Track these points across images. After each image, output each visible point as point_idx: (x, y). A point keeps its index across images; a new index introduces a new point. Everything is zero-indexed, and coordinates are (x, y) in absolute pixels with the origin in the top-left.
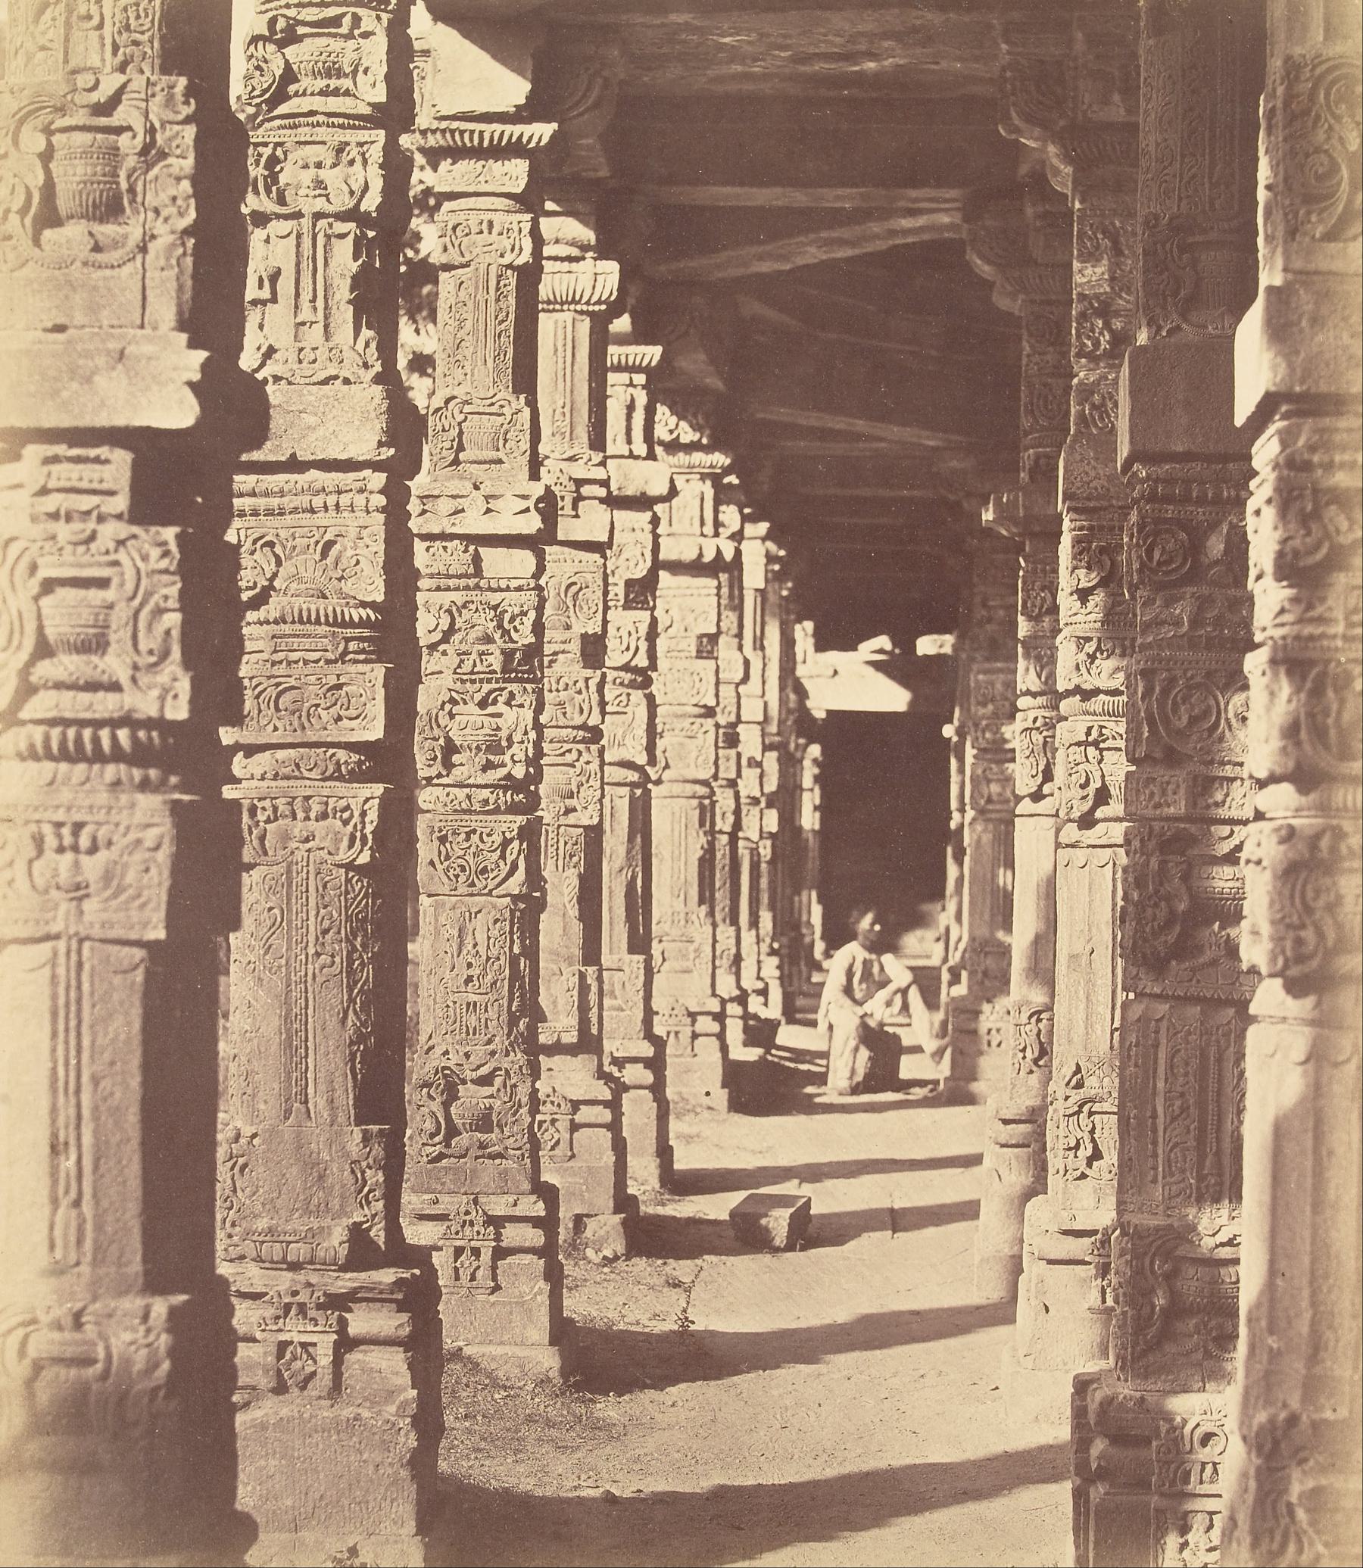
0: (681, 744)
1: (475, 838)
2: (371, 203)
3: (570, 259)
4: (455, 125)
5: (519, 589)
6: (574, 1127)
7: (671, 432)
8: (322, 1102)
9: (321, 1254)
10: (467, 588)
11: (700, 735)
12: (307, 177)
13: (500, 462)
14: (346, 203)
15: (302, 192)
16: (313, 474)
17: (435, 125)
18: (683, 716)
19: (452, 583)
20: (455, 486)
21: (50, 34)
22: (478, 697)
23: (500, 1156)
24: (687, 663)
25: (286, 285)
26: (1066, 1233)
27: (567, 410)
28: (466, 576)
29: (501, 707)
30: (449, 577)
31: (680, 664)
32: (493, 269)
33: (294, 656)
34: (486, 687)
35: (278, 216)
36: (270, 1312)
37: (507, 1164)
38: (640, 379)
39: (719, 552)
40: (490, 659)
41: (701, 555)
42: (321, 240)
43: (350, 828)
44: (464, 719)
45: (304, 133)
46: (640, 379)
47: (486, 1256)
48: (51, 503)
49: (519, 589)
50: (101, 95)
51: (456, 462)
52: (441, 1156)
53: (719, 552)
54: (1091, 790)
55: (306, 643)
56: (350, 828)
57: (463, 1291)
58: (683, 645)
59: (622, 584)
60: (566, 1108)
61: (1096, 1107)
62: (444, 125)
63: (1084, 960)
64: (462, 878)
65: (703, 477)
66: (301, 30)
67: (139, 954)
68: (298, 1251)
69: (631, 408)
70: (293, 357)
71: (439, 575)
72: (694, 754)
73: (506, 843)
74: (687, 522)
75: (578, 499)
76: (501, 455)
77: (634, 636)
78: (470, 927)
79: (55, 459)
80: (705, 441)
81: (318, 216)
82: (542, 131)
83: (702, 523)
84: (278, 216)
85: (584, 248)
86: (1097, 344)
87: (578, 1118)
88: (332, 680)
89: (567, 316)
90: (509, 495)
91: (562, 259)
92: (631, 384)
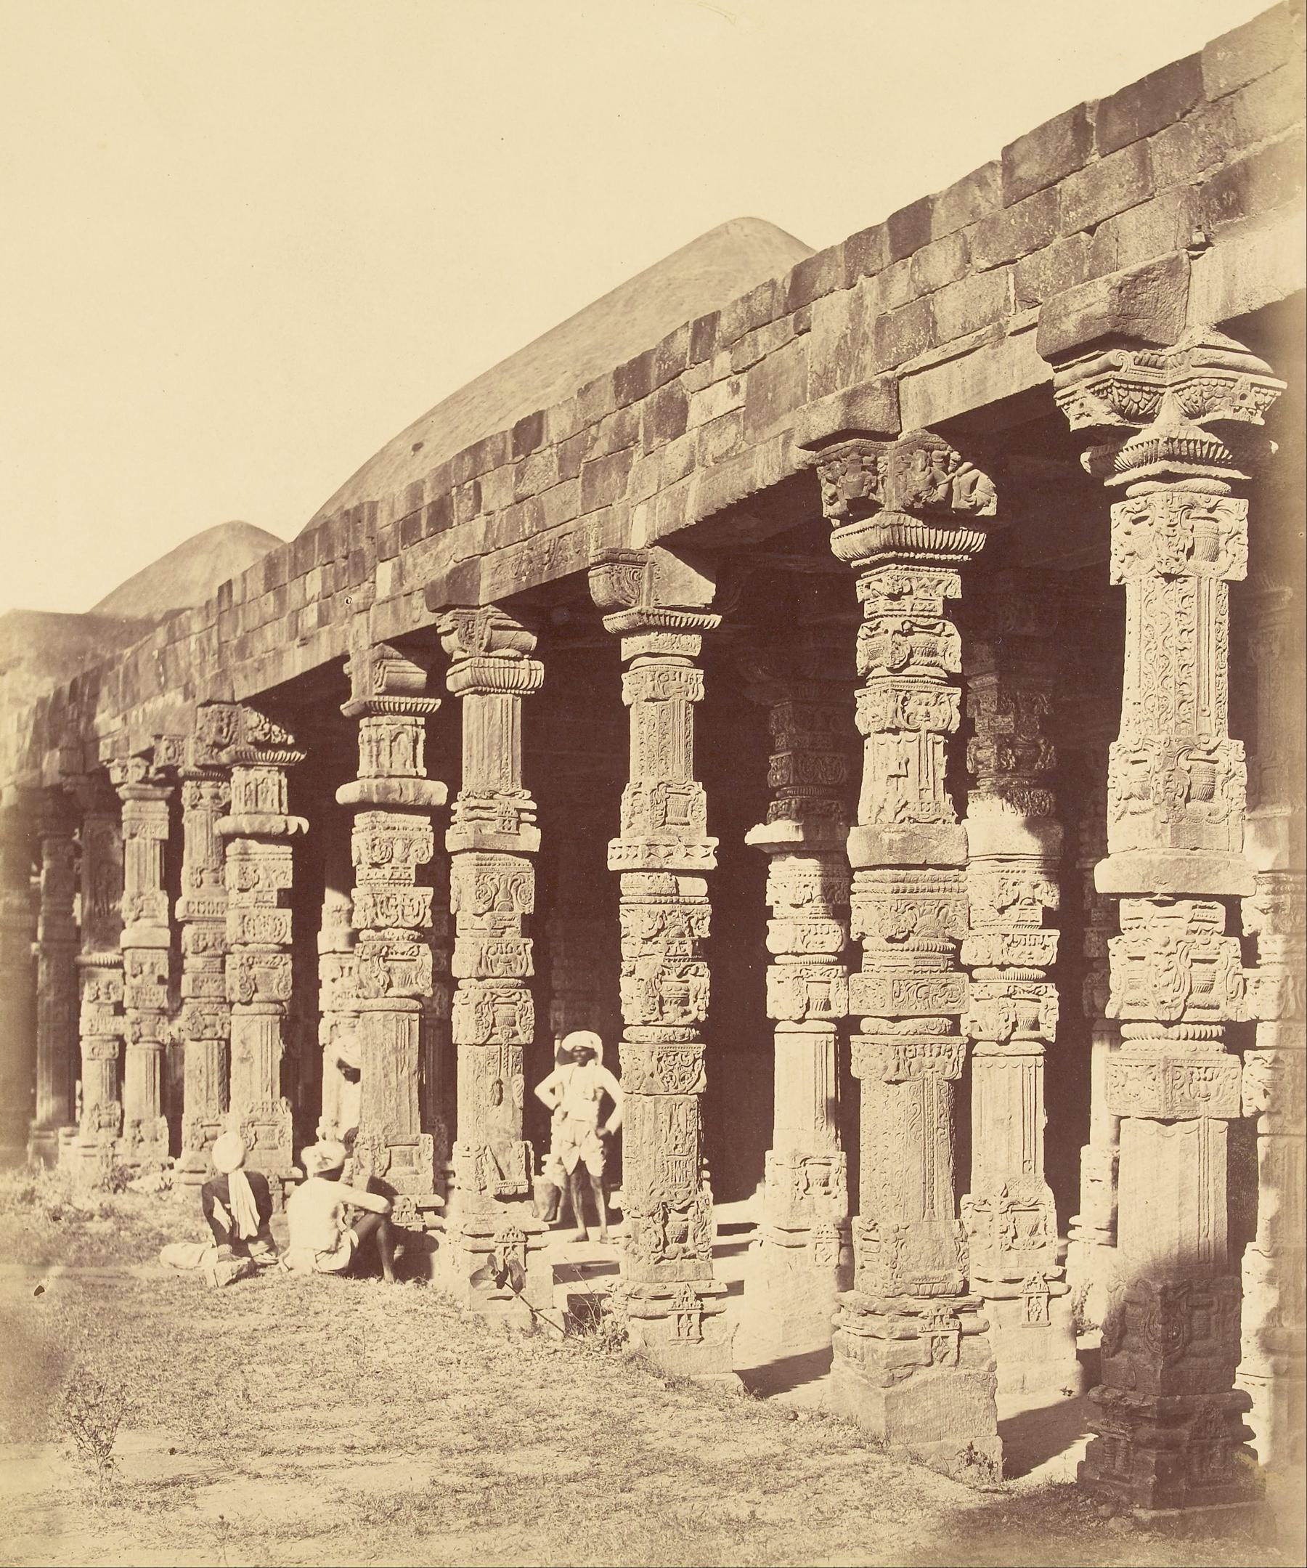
0: (267, 973)
1: (678, 1058)
2: (954, 727)
3: (515, 659)
4: (669, 612)
5: (700, 903)
6: (527, 1250)
7: (265, 735)
8: (941, 1207)
9: (950, 1287)
10: (672, 902)
11: (281, 967)
12: (922, 710)
13: (688, 824)
14: (941, 726)
15: (918, 717)
16: (930, 871)
17: (656, 611)
18: (268, 952)
19: (663, 899)
20: (666, 839)
21: (1189, 716)
22: (679, 970)
23: (694, 1256)
24: (271, 912)
25: (913, 767)
26: (1006, 1281)
27: (509, 761)
28: (671, 895)
29: (689, 977)
30: (660, 895)
31: (265, 912)
32: (683, 702)
33: (925, 968)
34: (683, 965)
35: (906, 729)
36: (927, 1321)
37: (697, 1261)
38: (421, 721)
39: (300, 826)
40: (684, 947)
41: (287, 829)
42: (930, 743)
43: (952, 1060)
44: (670, 984)
45: (919, 686)
46: (421, 721)
47: (696, 1318)
48: (1195, 926)
49: (700, 903)
50: (1210, 747)
51: (664, 824)
52: (662, 1258)
53: (300, 826)
54: (1010, 1023)
55: (931, 962)
56: (952, 1060)
57: (683, 1343)
58: (267, 897)
59: (413, 868)
60: (522, 1237)
61: (1015, 1207)
62: (662, 611)
63: (1006, 1122)
64: (671, 1084)
65: (280, 769)
66: (915, 629)
67: (1226, 1124)
68: (939, 1288)
69: (416, 741)
70: (918, 807)
71: (655, 894)
72: (276, 981)
73: (695, 1060)
74: (269, 802)
75: (520, 822)
76: (688, 819)
77: (422, 906)
78: (675, 1115)
79: (1194, 907)
80: (291, 740)
81: (929, 731)
82: (716, 619)
83: (281, 805)
84: (906, 729)
85: (524, 651)
86: (1008, 764)
87: (529, 1244)
88: (944, 982)
89: (509, 697)
90: (699, 846)
91: (508, 658)
92: (416, 725)
